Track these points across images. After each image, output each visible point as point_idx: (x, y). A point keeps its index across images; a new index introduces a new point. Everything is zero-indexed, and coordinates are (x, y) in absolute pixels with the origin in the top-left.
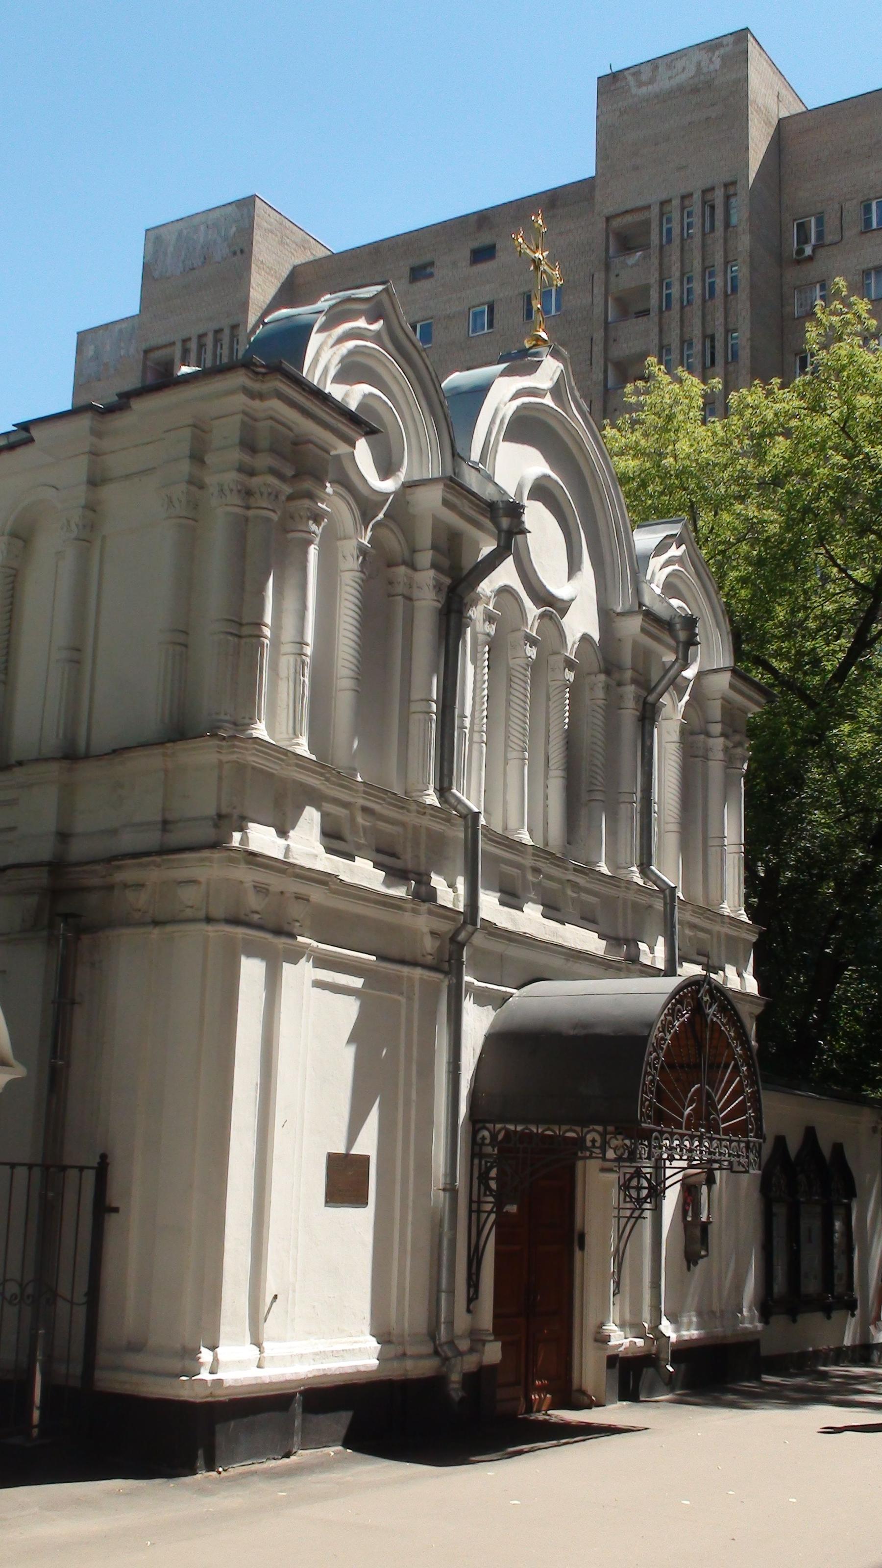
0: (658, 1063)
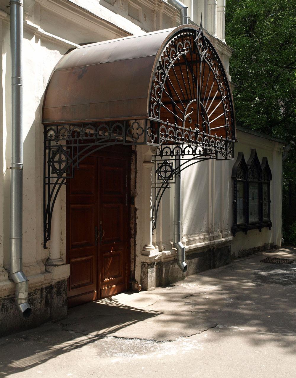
0: (164, 77)
